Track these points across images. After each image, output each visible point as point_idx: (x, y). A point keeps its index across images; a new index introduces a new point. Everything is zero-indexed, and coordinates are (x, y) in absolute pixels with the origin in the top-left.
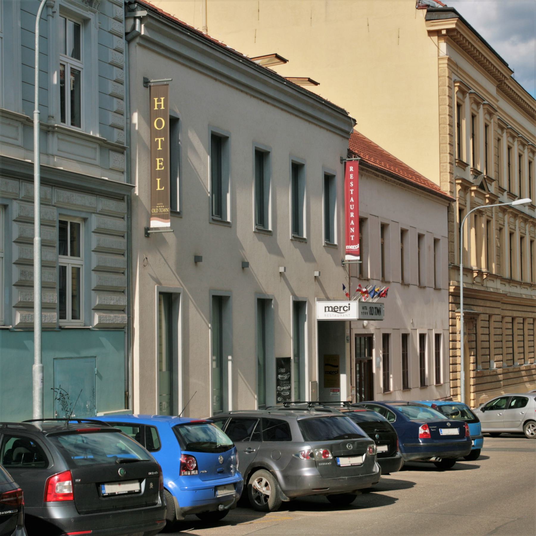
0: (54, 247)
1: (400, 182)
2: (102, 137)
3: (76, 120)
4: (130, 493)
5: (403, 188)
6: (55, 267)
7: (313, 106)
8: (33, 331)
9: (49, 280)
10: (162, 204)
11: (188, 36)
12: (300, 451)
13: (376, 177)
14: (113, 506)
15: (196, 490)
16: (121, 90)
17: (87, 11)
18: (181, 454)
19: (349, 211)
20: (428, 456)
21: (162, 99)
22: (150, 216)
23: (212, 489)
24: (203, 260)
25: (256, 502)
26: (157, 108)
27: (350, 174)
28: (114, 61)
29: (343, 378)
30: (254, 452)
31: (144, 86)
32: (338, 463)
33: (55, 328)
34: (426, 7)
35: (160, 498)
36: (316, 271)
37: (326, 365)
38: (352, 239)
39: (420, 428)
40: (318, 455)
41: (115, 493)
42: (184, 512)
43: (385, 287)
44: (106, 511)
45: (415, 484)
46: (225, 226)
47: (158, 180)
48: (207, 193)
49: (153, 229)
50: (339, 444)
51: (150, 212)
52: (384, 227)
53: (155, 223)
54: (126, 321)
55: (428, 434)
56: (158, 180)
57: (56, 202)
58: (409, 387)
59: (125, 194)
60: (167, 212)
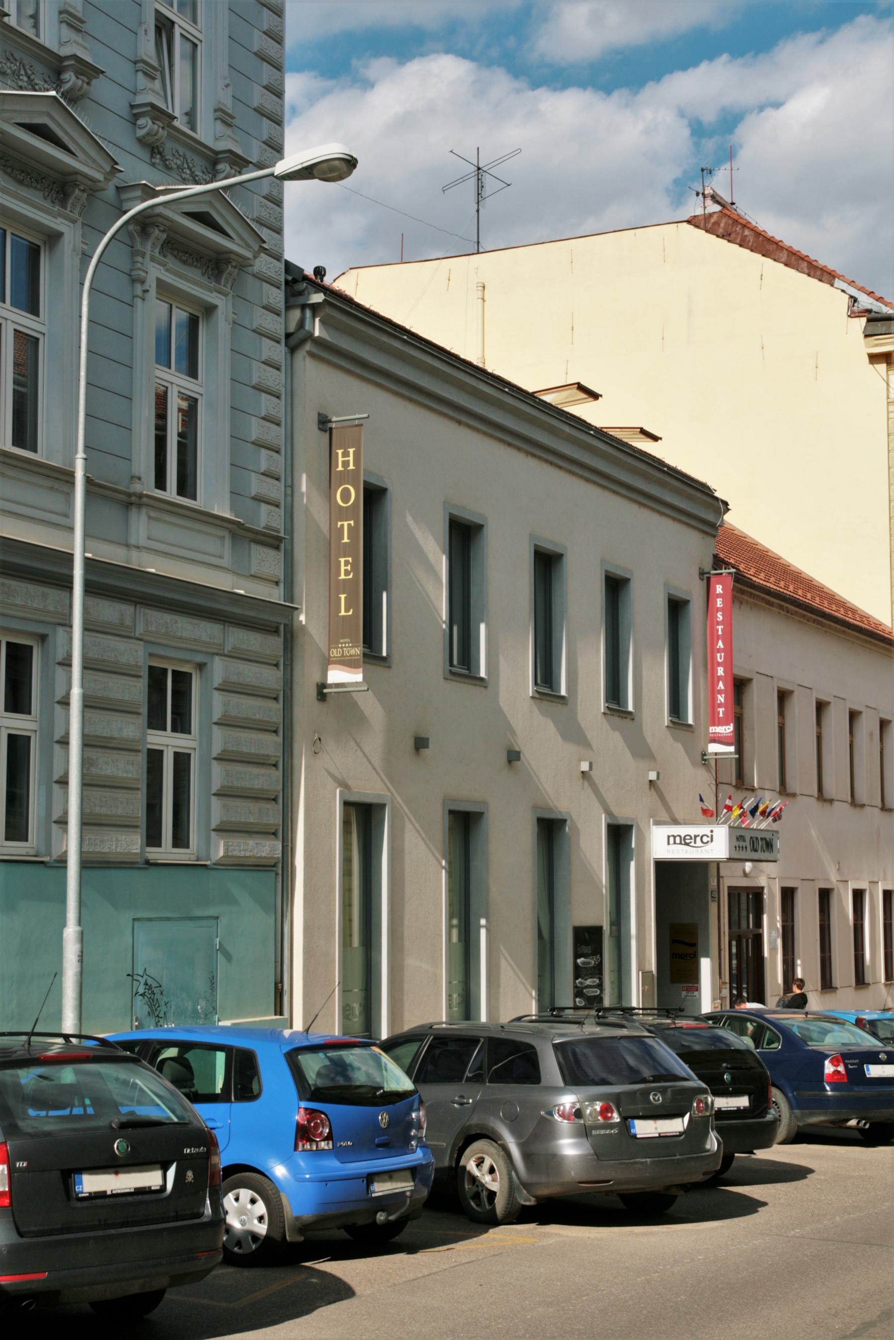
0: (139, 714)
1: (814, 617)
2: (236, 517)
3: (186, 486)
4: (140, 1191)
5: (820, 627)
6: (139, 751)
7: (645, 476)
8: (66, 867)
9: (125, 775)
10: (348, 640)
11: (405, 341)
12: (555, 1106)
13: (768, 606)
14: (99, 1221)
15: (326, 1181)
16: (275, 434)
17: (211, 292)
18: (299, 1108)
19: (716, 665)
20: (843, 1117)
21: (351, 451)
22: (326, 663)
23: (361, 1180)
24: (431, 746)
25: (472, 1203)
26: (342, 467)
27: (717, 597)
28: (263, 382)
29: (706, 965)
30: (469, 1103)
31: (320, 429)
32: (633, 1131)
33: (137, 863)
34: (866, 314)
35: (208, 1202)
36: (652, 770)
37: (674, 941)
38: (721, 715)
39: (827, 1062)
40: (591, 1114)
41: (105, 1192)
42: (303, 1226)
43: (753, 799)
44: (83, 1229)
45: (810, 1171)
46: (475, 685)
47: (343, 597)
48: (441, 622)
49: (331, 686)
50: (633, 1094)
51: (327, 655)
52: (783, 696)
53: (336, 676)
54: (278, 854)
55: (843, 1075)
56: (343, 597)
57: (142, 631)
58: (834, 985)
59: (280, 621)
60: (358, 655)
